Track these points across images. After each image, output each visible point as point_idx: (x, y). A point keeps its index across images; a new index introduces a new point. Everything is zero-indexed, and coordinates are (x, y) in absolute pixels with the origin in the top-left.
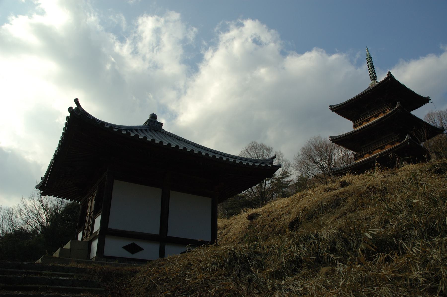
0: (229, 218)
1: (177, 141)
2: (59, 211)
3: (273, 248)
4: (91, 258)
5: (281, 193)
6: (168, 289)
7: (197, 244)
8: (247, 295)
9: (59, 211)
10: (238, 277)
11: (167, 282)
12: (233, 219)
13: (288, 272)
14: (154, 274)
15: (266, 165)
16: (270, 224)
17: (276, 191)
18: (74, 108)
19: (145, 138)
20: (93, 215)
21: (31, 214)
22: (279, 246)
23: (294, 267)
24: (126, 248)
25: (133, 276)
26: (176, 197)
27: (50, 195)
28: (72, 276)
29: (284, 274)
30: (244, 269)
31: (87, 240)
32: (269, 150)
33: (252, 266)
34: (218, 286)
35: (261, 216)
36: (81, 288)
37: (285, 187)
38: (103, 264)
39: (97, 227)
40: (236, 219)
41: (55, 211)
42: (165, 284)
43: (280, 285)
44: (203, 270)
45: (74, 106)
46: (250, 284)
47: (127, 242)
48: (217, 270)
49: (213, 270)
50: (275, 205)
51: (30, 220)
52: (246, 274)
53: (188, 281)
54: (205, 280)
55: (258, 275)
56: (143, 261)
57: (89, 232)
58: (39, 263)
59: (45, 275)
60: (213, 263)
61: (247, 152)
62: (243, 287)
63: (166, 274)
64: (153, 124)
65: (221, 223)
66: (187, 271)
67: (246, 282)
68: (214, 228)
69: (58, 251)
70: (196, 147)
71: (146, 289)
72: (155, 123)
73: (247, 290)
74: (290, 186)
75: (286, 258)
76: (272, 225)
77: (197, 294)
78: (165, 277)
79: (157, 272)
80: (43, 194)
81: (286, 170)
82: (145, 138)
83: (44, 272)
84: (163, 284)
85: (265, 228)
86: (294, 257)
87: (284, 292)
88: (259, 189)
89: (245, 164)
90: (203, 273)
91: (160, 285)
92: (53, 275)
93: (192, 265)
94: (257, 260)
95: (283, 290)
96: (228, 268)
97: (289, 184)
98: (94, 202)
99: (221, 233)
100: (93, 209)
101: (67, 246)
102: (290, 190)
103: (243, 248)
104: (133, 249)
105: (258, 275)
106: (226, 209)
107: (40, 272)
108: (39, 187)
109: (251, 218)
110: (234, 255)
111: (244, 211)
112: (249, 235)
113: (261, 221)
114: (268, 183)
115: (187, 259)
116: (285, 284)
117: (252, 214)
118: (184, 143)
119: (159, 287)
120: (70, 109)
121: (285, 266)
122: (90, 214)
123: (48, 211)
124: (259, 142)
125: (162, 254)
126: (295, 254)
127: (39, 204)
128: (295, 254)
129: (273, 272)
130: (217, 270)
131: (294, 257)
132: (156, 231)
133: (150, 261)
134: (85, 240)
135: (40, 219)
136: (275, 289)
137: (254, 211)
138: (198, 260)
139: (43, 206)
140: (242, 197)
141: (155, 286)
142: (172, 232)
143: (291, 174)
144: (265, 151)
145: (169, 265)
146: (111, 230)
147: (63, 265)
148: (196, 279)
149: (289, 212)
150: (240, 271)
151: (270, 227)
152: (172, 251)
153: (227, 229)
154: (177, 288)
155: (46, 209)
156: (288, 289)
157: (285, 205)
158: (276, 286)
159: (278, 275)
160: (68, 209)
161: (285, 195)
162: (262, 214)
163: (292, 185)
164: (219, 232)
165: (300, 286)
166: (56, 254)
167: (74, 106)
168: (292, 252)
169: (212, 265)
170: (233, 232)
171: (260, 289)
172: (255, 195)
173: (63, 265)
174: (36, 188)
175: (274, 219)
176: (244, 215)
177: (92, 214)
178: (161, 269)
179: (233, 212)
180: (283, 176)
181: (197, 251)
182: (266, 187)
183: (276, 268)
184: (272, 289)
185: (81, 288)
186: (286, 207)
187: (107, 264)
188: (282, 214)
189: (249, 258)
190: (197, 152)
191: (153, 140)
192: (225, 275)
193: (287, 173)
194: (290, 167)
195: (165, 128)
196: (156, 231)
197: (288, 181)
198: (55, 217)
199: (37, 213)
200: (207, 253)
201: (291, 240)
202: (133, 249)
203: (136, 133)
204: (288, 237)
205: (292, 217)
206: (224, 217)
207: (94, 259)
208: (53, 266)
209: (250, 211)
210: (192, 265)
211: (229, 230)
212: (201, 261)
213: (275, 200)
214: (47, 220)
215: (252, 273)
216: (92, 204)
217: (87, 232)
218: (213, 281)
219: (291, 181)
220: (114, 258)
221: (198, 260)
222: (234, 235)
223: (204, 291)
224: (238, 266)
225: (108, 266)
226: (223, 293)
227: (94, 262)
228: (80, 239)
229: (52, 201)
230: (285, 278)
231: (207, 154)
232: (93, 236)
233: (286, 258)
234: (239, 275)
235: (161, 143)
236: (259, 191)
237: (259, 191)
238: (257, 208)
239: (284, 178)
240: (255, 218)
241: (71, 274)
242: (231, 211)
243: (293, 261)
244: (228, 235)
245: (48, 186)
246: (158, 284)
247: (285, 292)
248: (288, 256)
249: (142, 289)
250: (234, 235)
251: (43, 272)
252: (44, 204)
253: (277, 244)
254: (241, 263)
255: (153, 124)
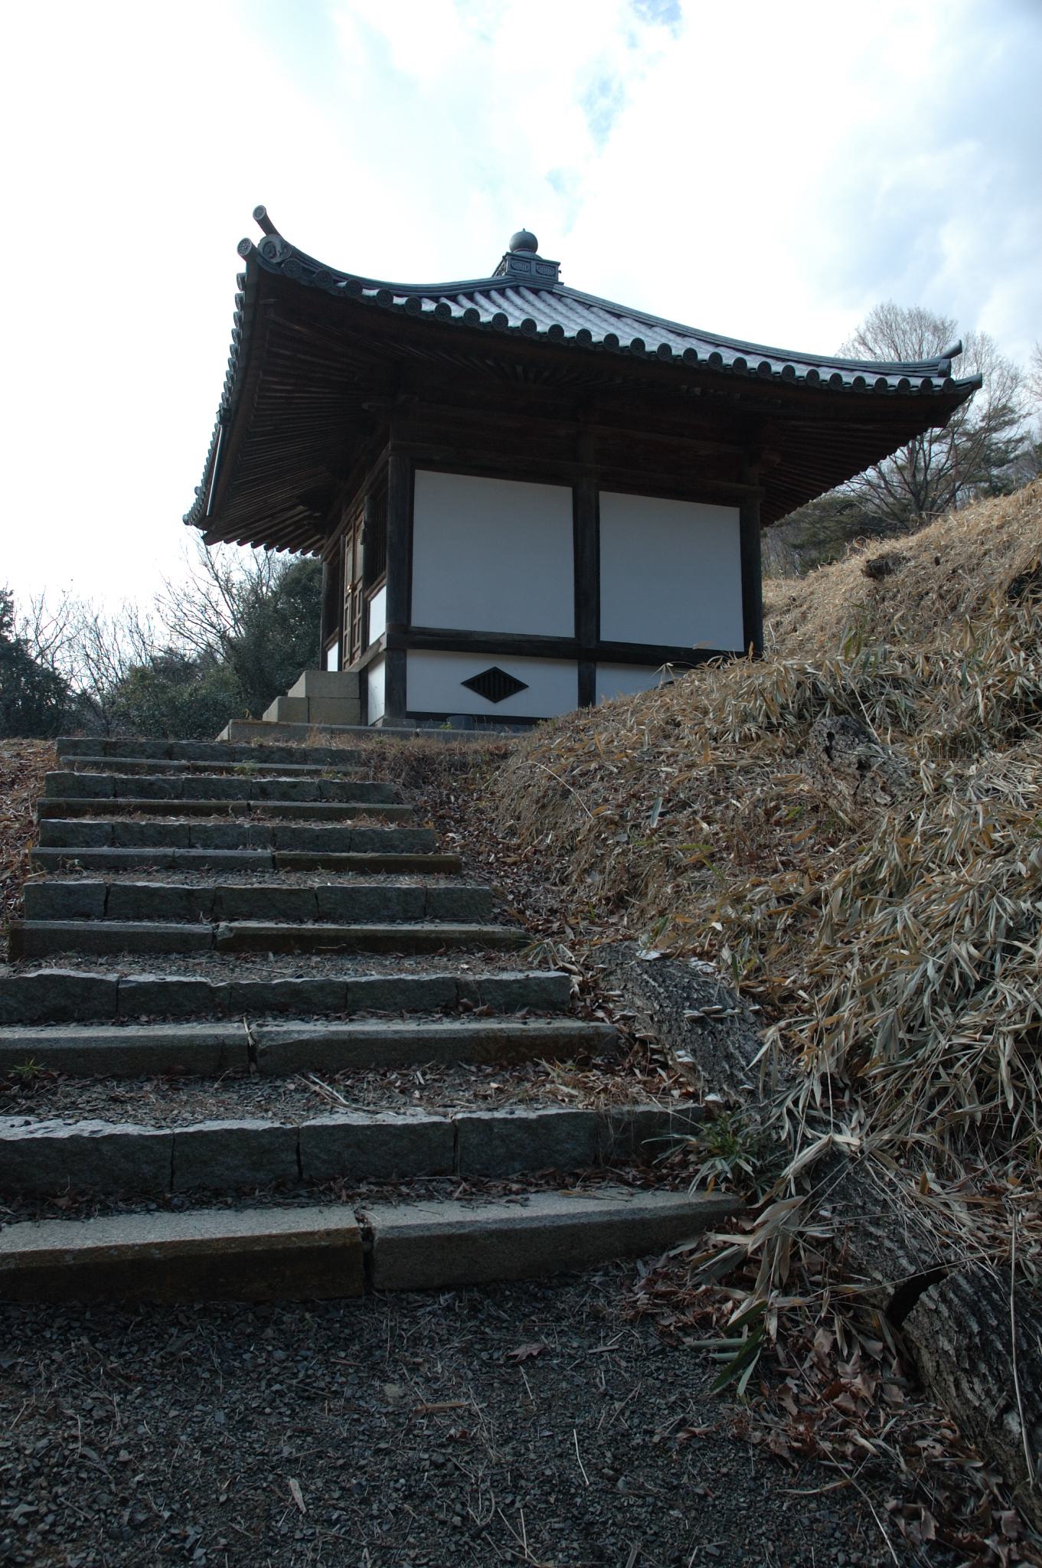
0: (804, 575)
1: (613, 320)
2: (264, 589)
3: (945, 662)
4: (371, 721)
5: (986, 485)
6: (606, 800)
7: (688, 659)
8: (854, 812)
9: (264, 589)
10: (825, 757)
11: (602, 779)
12: (817, 579)
13: (992, 737)
14: (559, 756)
15: (927, 382)
16: (941, 587)
17: (968, 479)
18: (256, 242)
19: (501, 319)
20: (363, 590)
21: (186, 606)
22: (966, 655)
23: (1014, 722)
24: (473, 684)
25: (498, 768)
26: (623, 517)
27: (227, 542)
28: (317, 772)
29: (981, 745)
30: (844, 728)
31: (354, 668)
32: (940, 330)
33: (873, 720)
34: (763, 785)
35: (912, 563)
36: (344, 805)
37: (1001, 463)
38: (405, 736)
39: (378, 626)
40: (827, 576)
41: (254, 591)
42: (594, 786)
43: (961, 776)
44: (715, 739)
45: (257, 236)
46: (863, 776)
47: (477, 666)
48: (759, 738)
49: (746, 739)
50: (961, 525)
51: (188, 624)
52: (851, 747)
53: (667, 773)
54: (721, 768)
55: (886, 747)
56: (527, 723)
57: (358, 644)
58: (223, 741)
59: (242, 771)
60: (745, 718)
61: (864, 343)
62: (842, 786)
63: (599, 755)
64: (527, 268)
65: (772, 592)
66: (665, 742)
67: (850, 771)
68: (753, 611)
69: (274, 707)
70: (679, 334)
71: (537, 802)
72: (533, 263)
73: (855, 794)
74: (1017, 458)
75: (989, 694)
76: (948, 591)
77: (695, 812)
78: (593, 766)
79: (570, 750)
80: (209, 540)
81: (1004, 400)
82: (501, 319)
83: (237, 765)
84: (588, 784)
85: (926, 602)
86: (1017, 690)
87: (974, 799)
88: (907, 474)
89: (852, 380)
90: (715, 749)
91: (581, 787)
92: (262, 772)
93: (678, 725)
94: (890, 704)
95: (971, 794)
96: (796, 730)
97: (1015, 449)
98: (360, 548)
99: (778, 624)
100: (360, 573)
101: (298, 690)
102: (1018, 471)
103: (841, 669)
104: (495, 686)
105: (886, 747)
106: (795, 547)
107: (226, 764)
108: (196, 518)
109: (877, 570)
110: (815, 689)
111: (854, 550)
112: (864, 627)
113: (910, 581)
114: (937, 452)
115: (661, 706)
116: (979, 776)
117: (882, 557)
118: (636, 325)
119: (577, 796)
120: (244, 247)
121: (985, 719)
122: (354, 589)
123: (234, 591)
124: (906, 305)
125: (587, 695)
126: (1020, 679)
127: (206, 575)
128: (1020, 679)
129: (942, 739)
130: (759, 738)
131: (1017, 690)
132: (564, 627)
133: (546, 720)
134: (348, 668)
135: (214, 619)
136: (946, 790)
137: (888, 546)
138: (696, 709)
139: (217, 578)
140: (847, 504)
141: (566, 794)
142: (611, 631)
143: (1023, 412)
144: (928, 336)
145: (606, 729)
146: (423, 631)
147: (290, 744)
148: (691, 766)
149: (1009, 545)
150: (830, 736)
151: (941, 597)
152: (615, 685)
153: (797, 611)
154: (634, 796)
155: (226, 588)
156: (987, 791)
157: (995, 523)
158: (949, 780)
159: (958, 747)
160: (294, 583)
161: (997, 490)
162: (914, 557)
163: (1026, 454)
164: (768, 624)
165: (1030, 778)
166: (271, 714)
167: (257, 236)
168: (1009, 673)
169: (744, 721)
170: (817, 621)
171: (895, 790)
172: (892, 495)
173: (290, 744)
174: (186, 523)
175: (954, 571)
176: (856, 562)
177: (360, 586)
178: (581, 740)
179: (815, 552)
180: (993, 423)
181: (692, 682)
182: (933, 465)
183: (952, 727)
184: (936, 790)
185: (344, 805)
186: (1000, 527)
187: (417, 735)
188: (985, 554)
189: (864, 697)
190: (681, 353)
191: (529, 324)
192: (784, 754)
193: (1005, 410)
194: (1018, 389)
195: (568, 278)
196: (564, 627)
197: (1009, 441)
198: (258, 611)
199: (203, 601)
200: (725, 686)
201: (1009, 635)
202: (495, 686)
203: (469, 305)
204: (996, 623)
205: (1017, 562)
206: (787, 575)
207: (379, 725)
208: (261, 746)
209: (875, 549)
210: (678, 725)
211: (804, 615)
212: (706, 713)
213: (963, 508)
214: (236, 621)
215: (870, 741)
216: (355, 557)
217: (352, 645)
218: (745, 771)
219: (1021, 440)
220: (441, 718)
221: (696, 709)
222: (822, 629)
223: (718, 803)
224: (825, 722)
225: (421, 741)
226: (777, 808)
227: (379, 732)
228: (333, 665)
229: (245, 562)
230: (982, 755)
231: (716, 358)
232: (369, 655)
233: (989, 694)
234: (828, 750)
235: (557, 330)
236: (909, 479)
237: (909, 479)
238: (897, 538)
239: (995, 430)
240: (890, 572)
241: (313, 767)
242: (814, 554)
243: (1012, 703)
244: (802, 630)
245: (221, 514)
246: (573, 785)
247: (979, 798)
248: (994, 685)
249: (525, 802)
250: (822, 629)
251: (234, 764)
252: (220, 574)
253: (960, 649)
254: (837, 711)
255: (527, 268)
